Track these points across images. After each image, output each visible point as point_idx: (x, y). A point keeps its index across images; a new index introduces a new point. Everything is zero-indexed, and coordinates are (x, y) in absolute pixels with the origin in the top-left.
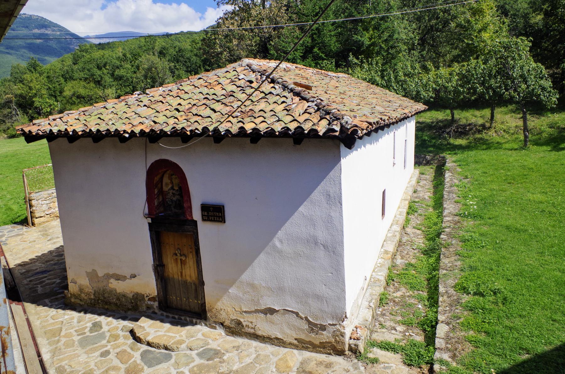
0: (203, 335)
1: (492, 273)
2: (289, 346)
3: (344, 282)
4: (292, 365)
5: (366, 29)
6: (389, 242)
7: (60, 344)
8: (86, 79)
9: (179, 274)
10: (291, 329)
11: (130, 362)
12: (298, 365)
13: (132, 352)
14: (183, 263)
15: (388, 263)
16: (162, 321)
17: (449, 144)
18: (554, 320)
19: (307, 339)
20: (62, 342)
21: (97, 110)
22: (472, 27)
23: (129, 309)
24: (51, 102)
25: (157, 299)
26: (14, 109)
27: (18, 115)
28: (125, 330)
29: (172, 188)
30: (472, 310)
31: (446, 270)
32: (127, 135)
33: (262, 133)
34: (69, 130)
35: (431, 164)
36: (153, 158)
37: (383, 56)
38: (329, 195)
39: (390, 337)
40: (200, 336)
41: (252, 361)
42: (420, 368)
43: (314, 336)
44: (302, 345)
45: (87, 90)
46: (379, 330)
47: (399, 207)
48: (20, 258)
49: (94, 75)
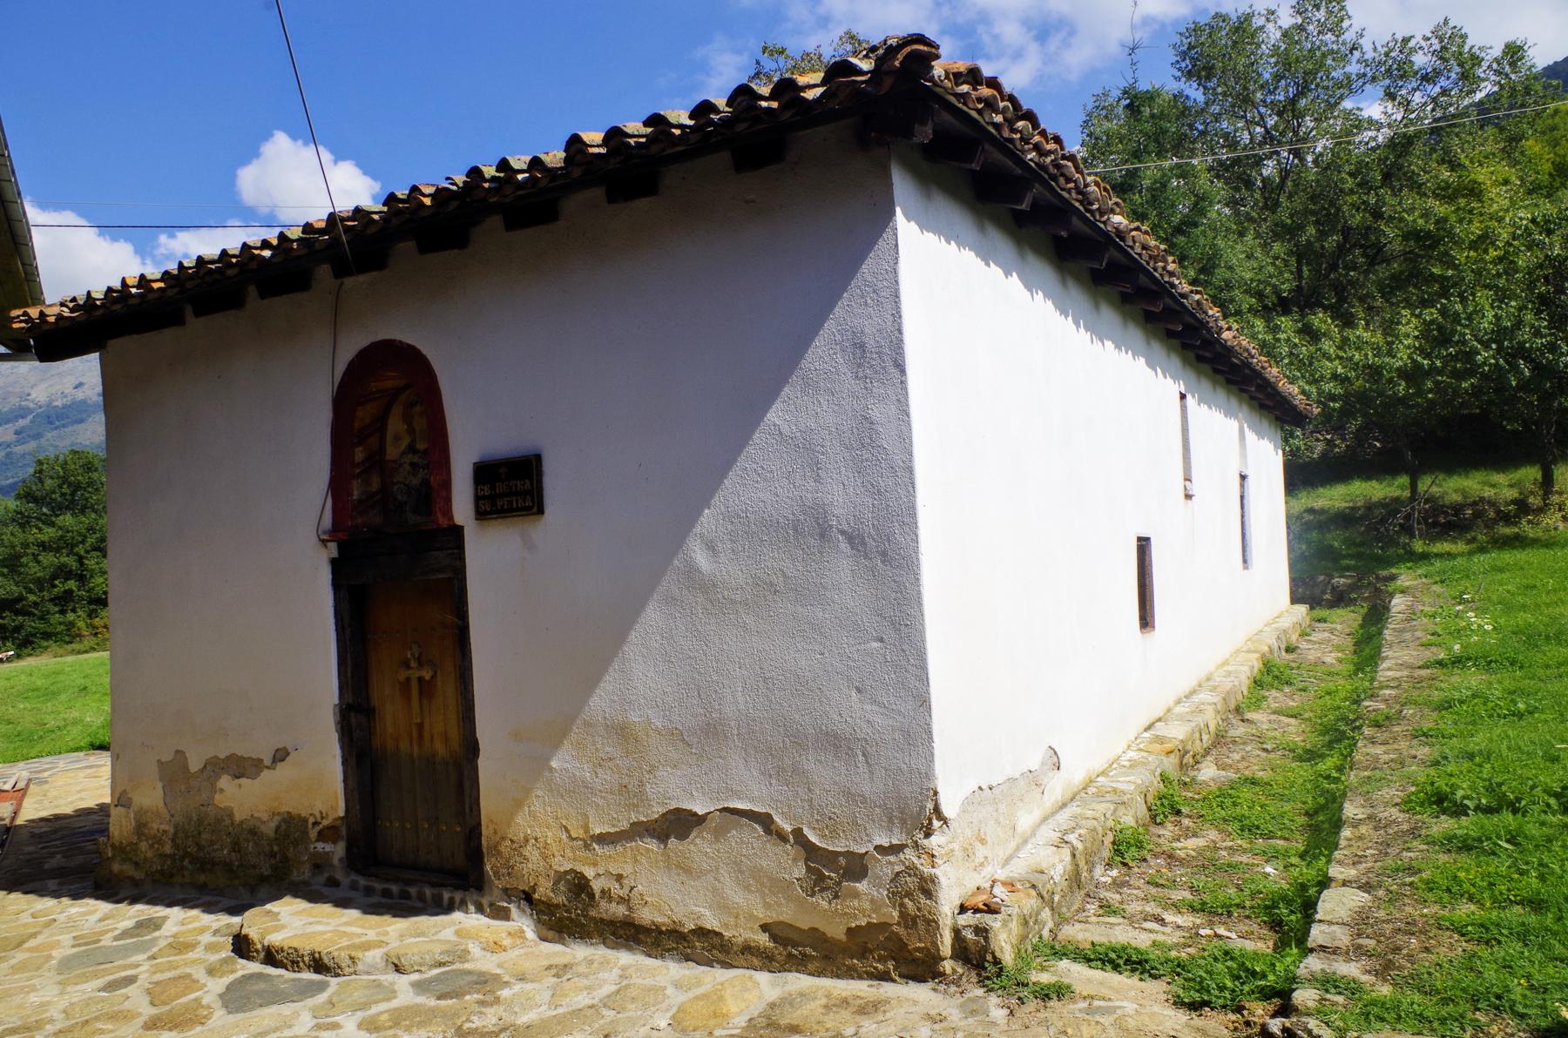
0: (457, 933)
2: (741, 960)
3: (923, 667)
4: (734, 1009)
9: (415, 735)
10: (747, 888)
11: (183, 1000)
16: (343, 903)
19: (804, 923)
25: (344, 832)
29: (411, 449)
30: (1469, 848)
35: (1352, 602)
36: (350, 347)
38: (862, 346)
41: (595, 1002)
42: (1239, 1009)
43: (825, 904)
44: (790, 949)
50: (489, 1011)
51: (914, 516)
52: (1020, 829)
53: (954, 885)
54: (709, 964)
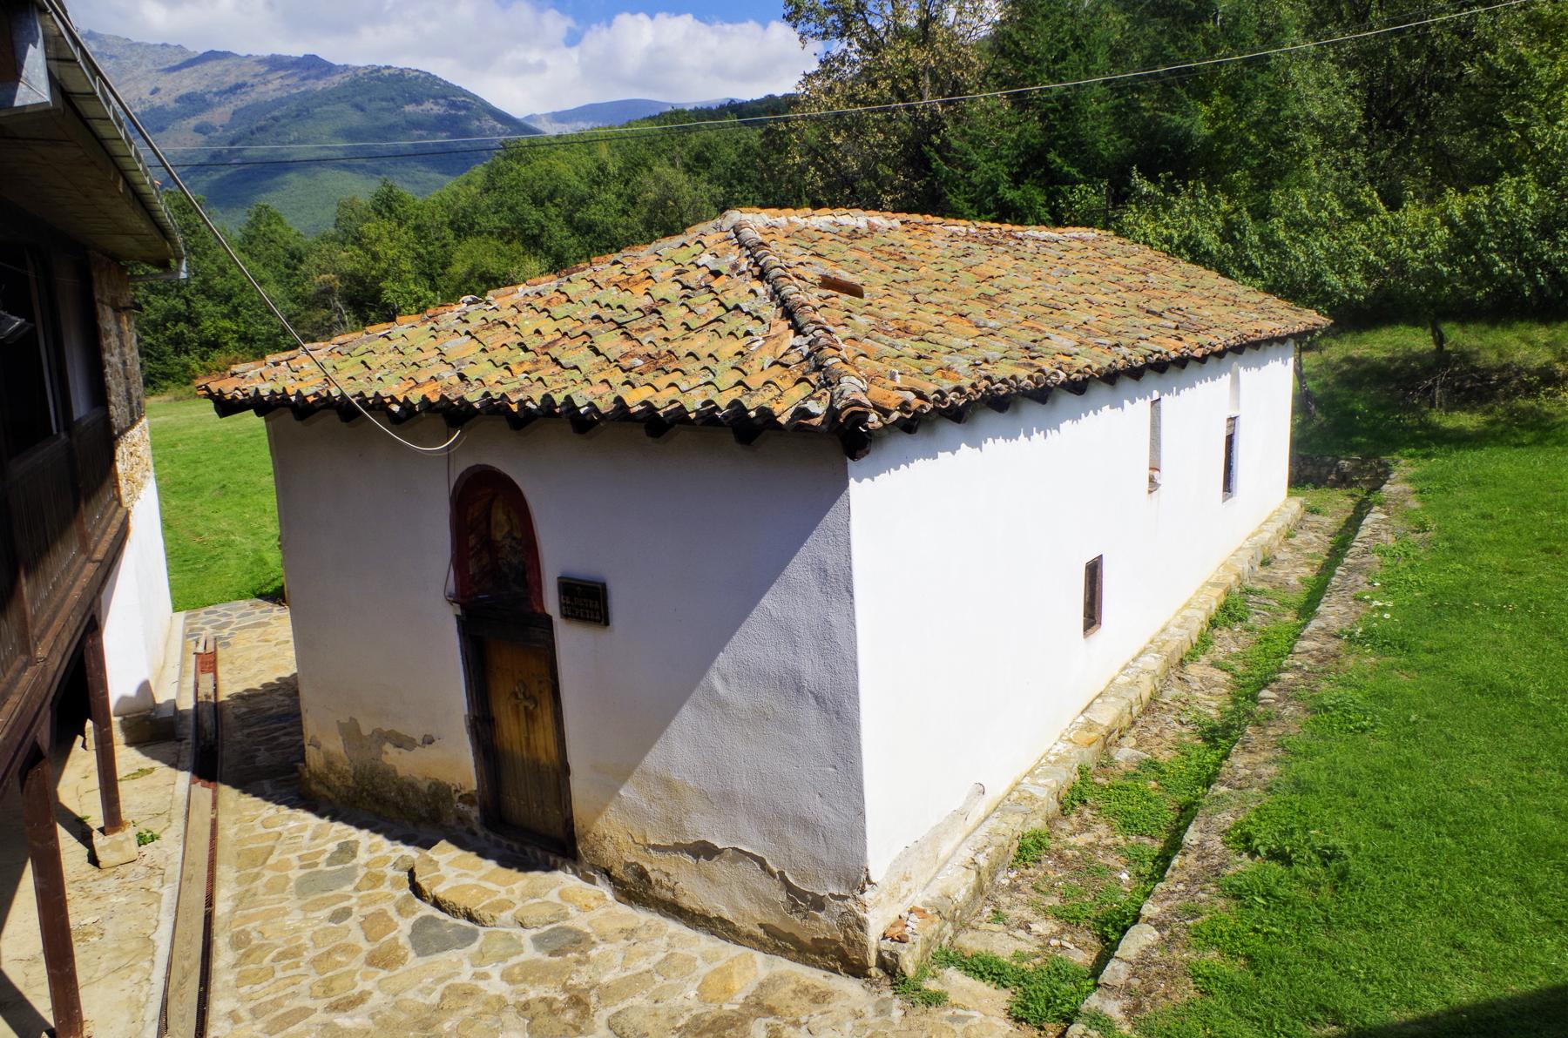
0: (561, 895)
1: (1350, 802)
2: (746, 942)
4: (737, 987)
5: (1205, 97)
6: (1112, 699)
7: (258, 882)
8: (503, 233)
11: (386, 938)
12: (751, 987)
13: (396, 918)
14: (531, 717)
15: (1089, 756)
16: (483, 854)
17: (1426, 426)
18: (1459, 946)
20: (265, 880)
21: (369, 340)
22: (1530, 74)
23: (422, 819)
24: (420, 291)
26: (337, 310)
27: (344, 323)
28: (401, 865)
30: (1239, 897)
31: (1230, 786)
32: (396, 408)
33: (661, 413)
34: (290, 391)
35: (1351, 484)
37: (1249, 168)
39: (1003, 946)
40: (553, 896)
44: (777, 942)
45: (504, 260)
46: (983, 926)
47: (1188, 605)
48: (245, 680)
49: (526, 221)
50: (583, 969)
51: (857, 693)
52: (941, 856)
53: (877, 922)
54: (726, 939)
